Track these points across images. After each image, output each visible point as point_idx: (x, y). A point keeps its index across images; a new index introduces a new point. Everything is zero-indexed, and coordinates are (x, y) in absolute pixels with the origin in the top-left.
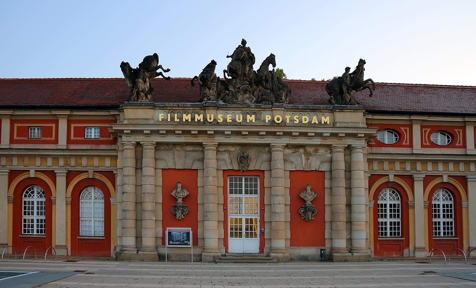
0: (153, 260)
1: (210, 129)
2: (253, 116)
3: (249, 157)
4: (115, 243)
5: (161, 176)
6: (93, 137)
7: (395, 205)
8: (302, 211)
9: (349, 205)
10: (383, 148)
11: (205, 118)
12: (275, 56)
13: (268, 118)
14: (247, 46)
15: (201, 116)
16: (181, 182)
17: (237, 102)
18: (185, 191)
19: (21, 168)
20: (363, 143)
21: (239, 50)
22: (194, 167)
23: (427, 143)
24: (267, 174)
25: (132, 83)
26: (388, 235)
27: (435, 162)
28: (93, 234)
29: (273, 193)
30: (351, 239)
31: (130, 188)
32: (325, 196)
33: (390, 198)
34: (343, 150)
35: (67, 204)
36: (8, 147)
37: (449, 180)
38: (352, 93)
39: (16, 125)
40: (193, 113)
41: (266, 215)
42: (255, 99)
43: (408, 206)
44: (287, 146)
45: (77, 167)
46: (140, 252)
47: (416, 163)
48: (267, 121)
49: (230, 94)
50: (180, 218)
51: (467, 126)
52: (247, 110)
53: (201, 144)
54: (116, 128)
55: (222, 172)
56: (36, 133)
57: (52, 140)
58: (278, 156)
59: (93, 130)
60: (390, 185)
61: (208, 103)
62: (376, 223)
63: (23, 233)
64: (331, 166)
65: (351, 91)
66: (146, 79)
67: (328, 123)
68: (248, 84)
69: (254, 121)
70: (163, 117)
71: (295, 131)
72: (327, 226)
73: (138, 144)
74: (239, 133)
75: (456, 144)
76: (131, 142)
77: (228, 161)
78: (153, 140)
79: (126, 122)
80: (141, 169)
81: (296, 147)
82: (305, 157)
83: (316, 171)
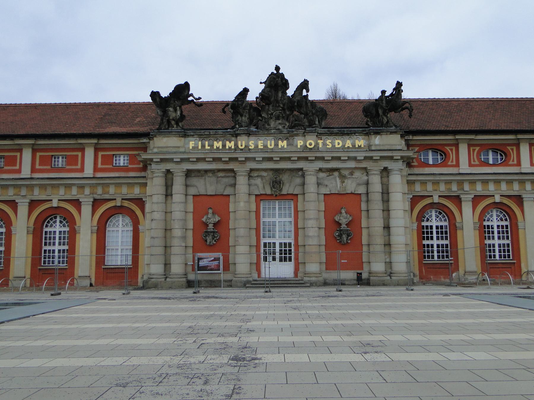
0: (180, 287)
1: (241, 157)
2: (285, 142)
3: (281, 182)
4: (143, 272)
5: (192, 202)
6: (122, 164)
7: (442, 227)
8: (337, 234)
9: (387, 227)
10: (427, 169)
11: (236, 145)
12: (308, 82)
13: (300, 143)
14: (280, 72)
15: (233, 143)
16: (212, 208)
17: (269, 128)
18: (216, 216)
19: (44, 197)
20: (400, 165)
21: (271, 77)
22: (295, 193)
23: (475, 162)
24: (300, 198)
25: (162, 111)
26: (436, 258)
27: (485, 182)
28: (119, 264)
29: (306, 217)
30: (391, 262)
31: (158, 216)
32: (361, 218)
33: (436, 219)
34: (379, 172)
35: (92, 232)
36: (29, 176)
37: (501, 200)
38: (389, 115)
39: (38, 154)
40: (225, 140)
41: (300, 239)
42: (288, 124)
43: (456, 227)
44: (321, 170)
45: (105, 195)
46: (168, 279)
47: (463, 182)
48: (299, 147)
49: (263, 120)
50: (211, 243)
51: (521, 144)
52: (279, 136)
53: (232, 171)
54: (145, 156)
55: (254, 197)
56: (60, 162)
57: (77, 169)
58: (311, 180)
59: (122, 158)
60: (435, 206)
61: (239, 130)
62: (422, 247)
63: (42, 265)
64: (367, 188)
65: (388, 114)
66: (176, 107)
67: (362, 146)
68: (281, 110)
69: (285, 147)
70: (193, 145)
71: (328, 156)
72: (365, 249)
73: (168, 171)
74: (270, 159)
75: (509, 162)
76: (160, 169)
77: (261, 186)
78: (184, 167)
79: (155, 150)
80: (172, 195)
81: (331, 171)
82: (340, 180)
83: (352, 193)
